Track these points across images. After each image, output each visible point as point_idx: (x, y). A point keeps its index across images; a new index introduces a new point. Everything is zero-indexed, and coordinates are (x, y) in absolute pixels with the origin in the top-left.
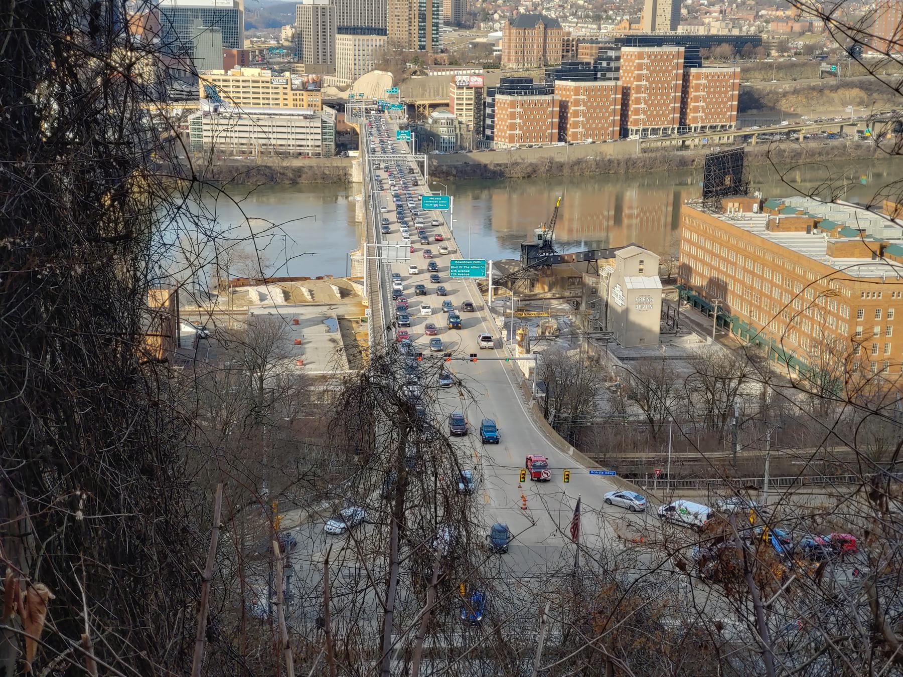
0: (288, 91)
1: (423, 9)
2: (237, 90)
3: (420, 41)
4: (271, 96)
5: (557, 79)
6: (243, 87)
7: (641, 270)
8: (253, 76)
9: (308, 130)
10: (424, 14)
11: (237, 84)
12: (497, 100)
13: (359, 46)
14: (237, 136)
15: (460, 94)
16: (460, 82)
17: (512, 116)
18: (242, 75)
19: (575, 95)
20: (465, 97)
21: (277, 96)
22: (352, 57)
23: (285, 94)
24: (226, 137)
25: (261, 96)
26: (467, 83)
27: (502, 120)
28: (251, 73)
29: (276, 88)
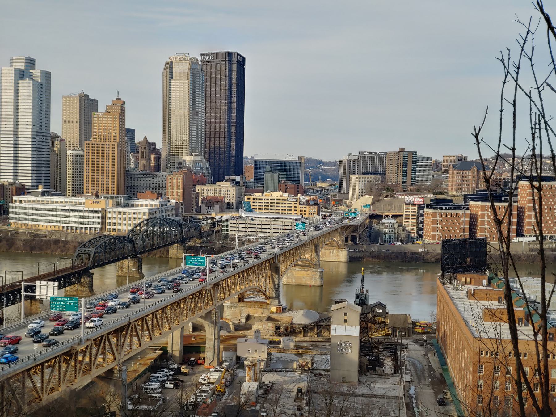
0: (298, 205)
2: (267, 204)
3: (403, 179)
4: (258, 204)
5: (470, 201)
6: (271, 203)
7: (345, 321)
8: (277, 196)
9: (281, 227)
10: (407, 163)
11: (267, 201)
12: (425, 212)
15: (408, 209)
16: (407, 201)
17: (434, 222)
18: (271, 196)
19: (481, 211)
20: (411, 210)
21: (290, 209)
22: (358, 188)
25: (281, 208)
26: (412, 202)
27: (428, 225)
29: (290, 204)
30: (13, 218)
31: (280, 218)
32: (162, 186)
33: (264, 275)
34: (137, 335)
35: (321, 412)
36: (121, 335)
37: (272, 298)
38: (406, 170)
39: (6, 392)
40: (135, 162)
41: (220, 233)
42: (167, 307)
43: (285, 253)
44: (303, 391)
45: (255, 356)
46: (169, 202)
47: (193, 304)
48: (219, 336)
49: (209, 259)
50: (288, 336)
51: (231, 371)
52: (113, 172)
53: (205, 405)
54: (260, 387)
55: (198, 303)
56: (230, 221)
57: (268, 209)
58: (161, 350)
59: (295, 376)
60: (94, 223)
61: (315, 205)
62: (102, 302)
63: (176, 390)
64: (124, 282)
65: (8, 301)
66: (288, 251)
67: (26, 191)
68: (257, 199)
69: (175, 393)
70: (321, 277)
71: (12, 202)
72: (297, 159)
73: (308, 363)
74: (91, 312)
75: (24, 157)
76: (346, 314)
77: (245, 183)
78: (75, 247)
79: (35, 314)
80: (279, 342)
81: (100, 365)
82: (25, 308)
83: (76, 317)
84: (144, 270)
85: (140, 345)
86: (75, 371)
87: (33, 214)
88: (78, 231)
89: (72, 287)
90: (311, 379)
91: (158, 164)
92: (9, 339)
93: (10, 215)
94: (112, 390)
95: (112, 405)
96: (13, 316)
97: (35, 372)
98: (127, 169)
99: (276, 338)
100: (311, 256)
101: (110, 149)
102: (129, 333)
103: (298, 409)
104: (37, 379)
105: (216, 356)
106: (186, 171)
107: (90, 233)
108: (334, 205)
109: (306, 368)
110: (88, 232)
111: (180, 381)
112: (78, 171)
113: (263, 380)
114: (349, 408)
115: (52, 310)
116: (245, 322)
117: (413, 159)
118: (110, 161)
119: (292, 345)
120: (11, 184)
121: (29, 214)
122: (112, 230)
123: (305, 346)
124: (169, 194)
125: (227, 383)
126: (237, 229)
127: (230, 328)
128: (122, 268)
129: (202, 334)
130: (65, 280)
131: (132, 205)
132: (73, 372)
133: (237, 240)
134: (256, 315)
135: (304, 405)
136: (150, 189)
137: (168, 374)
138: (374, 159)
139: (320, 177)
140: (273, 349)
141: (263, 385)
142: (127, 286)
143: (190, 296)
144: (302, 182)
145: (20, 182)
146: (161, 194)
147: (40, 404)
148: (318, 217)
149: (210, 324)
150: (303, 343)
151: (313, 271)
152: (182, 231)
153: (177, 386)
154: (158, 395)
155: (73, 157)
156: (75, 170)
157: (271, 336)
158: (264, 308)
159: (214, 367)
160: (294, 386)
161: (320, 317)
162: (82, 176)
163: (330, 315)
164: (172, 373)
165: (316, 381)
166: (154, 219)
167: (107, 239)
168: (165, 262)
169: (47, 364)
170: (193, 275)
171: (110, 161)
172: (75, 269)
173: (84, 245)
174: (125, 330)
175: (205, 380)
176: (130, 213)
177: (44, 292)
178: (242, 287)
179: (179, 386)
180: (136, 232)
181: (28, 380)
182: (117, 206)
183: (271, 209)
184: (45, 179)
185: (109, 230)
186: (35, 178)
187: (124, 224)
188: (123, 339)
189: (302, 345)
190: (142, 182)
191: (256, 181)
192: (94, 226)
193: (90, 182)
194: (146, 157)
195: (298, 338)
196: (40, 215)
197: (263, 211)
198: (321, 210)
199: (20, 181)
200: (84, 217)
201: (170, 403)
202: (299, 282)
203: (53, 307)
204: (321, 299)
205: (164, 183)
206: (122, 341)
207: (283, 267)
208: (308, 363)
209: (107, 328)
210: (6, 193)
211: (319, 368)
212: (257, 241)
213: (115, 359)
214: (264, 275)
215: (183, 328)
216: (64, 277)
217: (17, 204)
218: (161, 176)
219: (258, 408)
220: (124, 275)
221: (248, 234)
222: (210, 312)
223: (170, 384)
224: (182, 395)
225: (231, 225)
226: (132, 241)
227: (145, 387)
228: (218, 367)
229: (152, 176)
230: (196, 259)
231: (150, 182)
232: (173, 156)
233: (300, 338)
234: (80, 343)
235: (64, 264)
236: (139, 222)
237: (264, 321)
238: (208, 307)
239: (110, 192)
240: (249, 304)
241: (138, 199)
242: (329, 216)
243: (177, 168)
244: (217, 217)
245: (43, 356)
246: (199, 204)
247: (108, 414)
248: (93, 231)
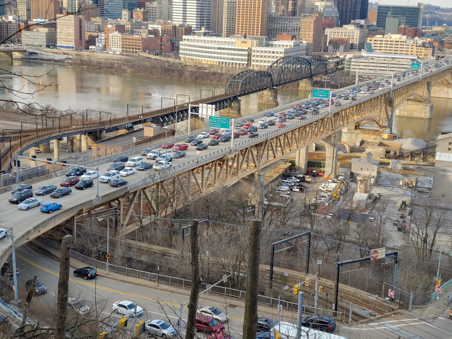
4: (378, 45)
7: (449, 149)
8: (396, 38)
9: (398, 66)
18: (391, 38)
29: (408, 45)
30: (182, 54)
32: (297, 29)
33: (379, 107)
34: (273, 150)
35: (421, 220)
36: (260, 148)
37: (385, 127)
39: (176, 184)
40: (276, 7)
41: (343, 71)
42: (296, 129)
43: (400, 88)
44: (407, 203)
45: (367, 173)
46: (301, 42)
47: (317, 129)
48: (337, 155)
49: (331, 92)
50: (397, 159)
51: (346, 183)
52: (258, 16)
53: (323, 207)
54: (370, 197)
55: (320, 128)
56: (353, 60)
57: (387, 50)
58: (290, 162)
59: (401, 191)
60: (242, 60)
61: (430, 47)
62: (248, 123)
63: (302, 194)
64: (263, 108)
65: (179, 118)
66: (402, 87)
67: (193, 31)
68: (378, 41)
69: (300, 196)
70: (431, 110)
71: (182, 41)
72: (417, 5)
73: (413, 182)
74: (239, 130)
75: (191, 3)
76: (450, 143)
77: (368, 26)
78: (228, 79)
79: (198, 128)
80: (388, 164)
81: (244, 170)
82: (191, 123)
83: (228, 133)
84: (279, 100)
85: (275, 157)
86: (227, 173)
87: (197, 51)
88: (230, 66)
89: (225, 109)
90: (414, 194)
91: (295, 9)
92: (180, 146)
93: (180, 51)
94: (253, 189)
95: (253, 200)
96: (182, 129)
97: (197, 171)
98: (269, 14)
99: (386, 161)
100: (423, 92)
102: (266, 148)
103: (401, 217)
104: (199, 176)
105: (333, 170)
106: (318, 16)
107: (239, 68)
108: (448, 48)
109: (411, 186)
110: (237, 66)
111: (304, 187)
112: (232, 15)
113: (372, 192)
114: (446, 220)
115: (211, 126)
116: (359, 145)
118: (257, 6)
119: (399, 167)
120: (181, 26)
121: (194, 51)
122: (255, 66)
123: (411, 168)
124: (302, 35)
125: (342, 192)
126: (358, 67)
127: (346, 149)
128: (262, 97)
129: (323, 153)
130: (220, 104)
131: (272, 45)
132: (225, 174)
133: (357, 77)
134: (369, 140)
135: (407, 214)
136: (286, 31)
137: (295, 181)
139: (437, 22)
140: (383, 169)
141: (372, 196)
142: (266, 111)
143: (314, 122)
144: (420, 26)
145: (188, 25)
146: (296, 36)
147: (201, 195)
148: (432, 58)
149: (330, 145)
150: (410, 166)
151: (423, 105)
152: (311, 69)
153: (301, 190)
154: (287, 196)
155: (228, 4)
156: (229, 15)
157: (381, 158)
158: (377, 135)
159: (331, 179)
160: (399, 200)
161: (427, 145)
162: (234, 20)
163: (436, 144)
164: (298, 180)
165: (419, 197)
166: (288, 57)
167: (251, 73)
168: (296, 93)
169: (206, 166)
170: (318, 105)
171: (257, 6)
172: (228, 96)
173: (235, 77)
174: (263, 145)
175: (324, 188)
176: (269, 52)
177: (204, 112)
178: (359, 117)
179: (303, 191)
180: (273, 68)
181: (193, 177)
182: (260, 46)
183: (390, 50)
184: (207, 22)
185: (253, 65)
186: (199, 21)
187: (265, 62)
188: (262, 151)
189: (408, 167)
190: (281, 25)
191: (378, 25)
192: (242, 62)
194: (285, 3)
195: (406, 161)
196: (203, 52)
197: (383, 51)
198: (435, 52)
199: (188, 23)
200: (235, 55)
201: (297, 203)
202: (410, 114)
203: (211, 124)
204: (429, 129)
205: (298, 26)
206: (261, 153)
207: (396, 101)
208: (413, 182)
209: (250, 143)
210: (177, 33)
211: (422, 186)
212: (375, 78)
213: (256, 166)
214: (379, 107)
215: (307, 147)
216: (219, 102)
217: (186, 42)
219: (367, 213)
220: (263, 102)
221: (367, 71)
222: (330, 136)
223: (296, 188)
224: (306, 198)
225: (353, 63)
226: (270, 75)
227: (278, 189)
228: (335, 179)
229: (289, 19)
230: (321, 92)
231: (287, 25)
232: (308, 2)
233: (408, 161)
234: (230, 152)
235: (220, 92)
236: (277, 59)
237: (376, 146)
238: (329, 132)
239: (255, 33)
240: (364, 131)
241: (276, 40)
242: (443, 57)
243: (310, 13)
244: (342, 57)
245: (203, 160)
246: (326, 45)
247: (250, 206)
248: (241, 66)
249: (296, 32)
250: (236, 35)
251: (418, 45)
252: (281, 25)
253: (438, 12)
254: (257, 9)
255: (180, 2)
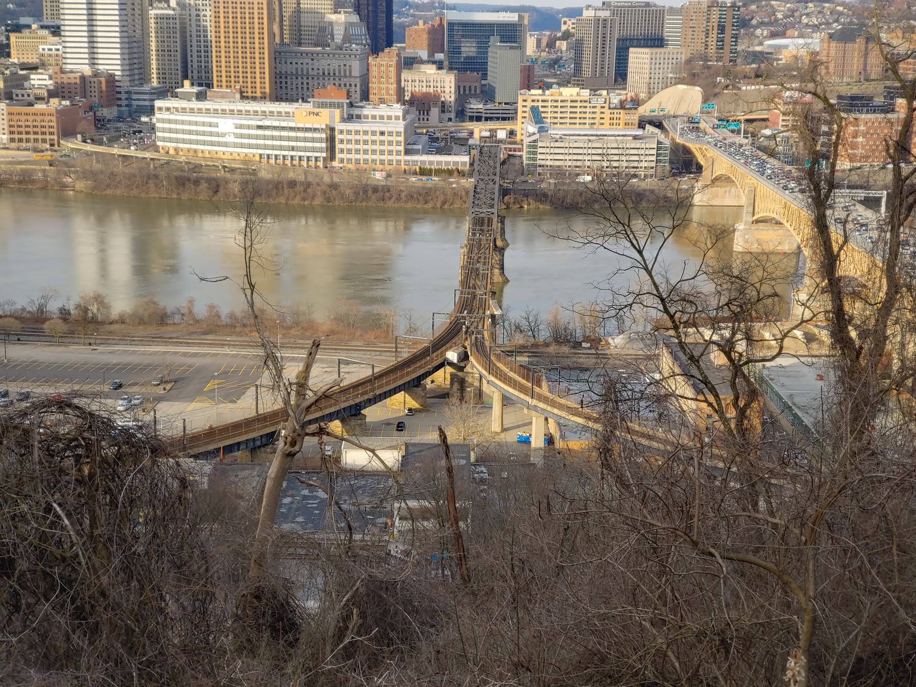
0: (606, 110)
1: (723, 20)
2: (556, 110)
4: (587, 115)
5: (898, 97)
8: (571, 95)
10: (724, 27)
11: (555, 104)
13: (656, 59)
14: (552, 158)
18: (561, 94)
21: (593, 116)
23: (602, 113)
24: (618, 161)
28: (569, 92)
29: (593, 107)
31: (606, 135)
32: (329, 74)
38: (724, 37)
60: (313, 150)
68: (538, 101)
101: (256, 11)
117: (734, 18)
118: (256, 31)
124: (374, 91)
131: (359, 117)
138: (628, 14)
171: (256, 31)
185: (342, 161)
190: (295, 66)
193: (223, 69)
210: (88, 89)
218: (326, 55)
221: (569, 163)
229: (310, 55)
249: (329, 79)
250: (215, 89)
251: (612, 106)
252: (295, 66)
253: (409, 9)
254: (257, 36)
255: (81, 26)
